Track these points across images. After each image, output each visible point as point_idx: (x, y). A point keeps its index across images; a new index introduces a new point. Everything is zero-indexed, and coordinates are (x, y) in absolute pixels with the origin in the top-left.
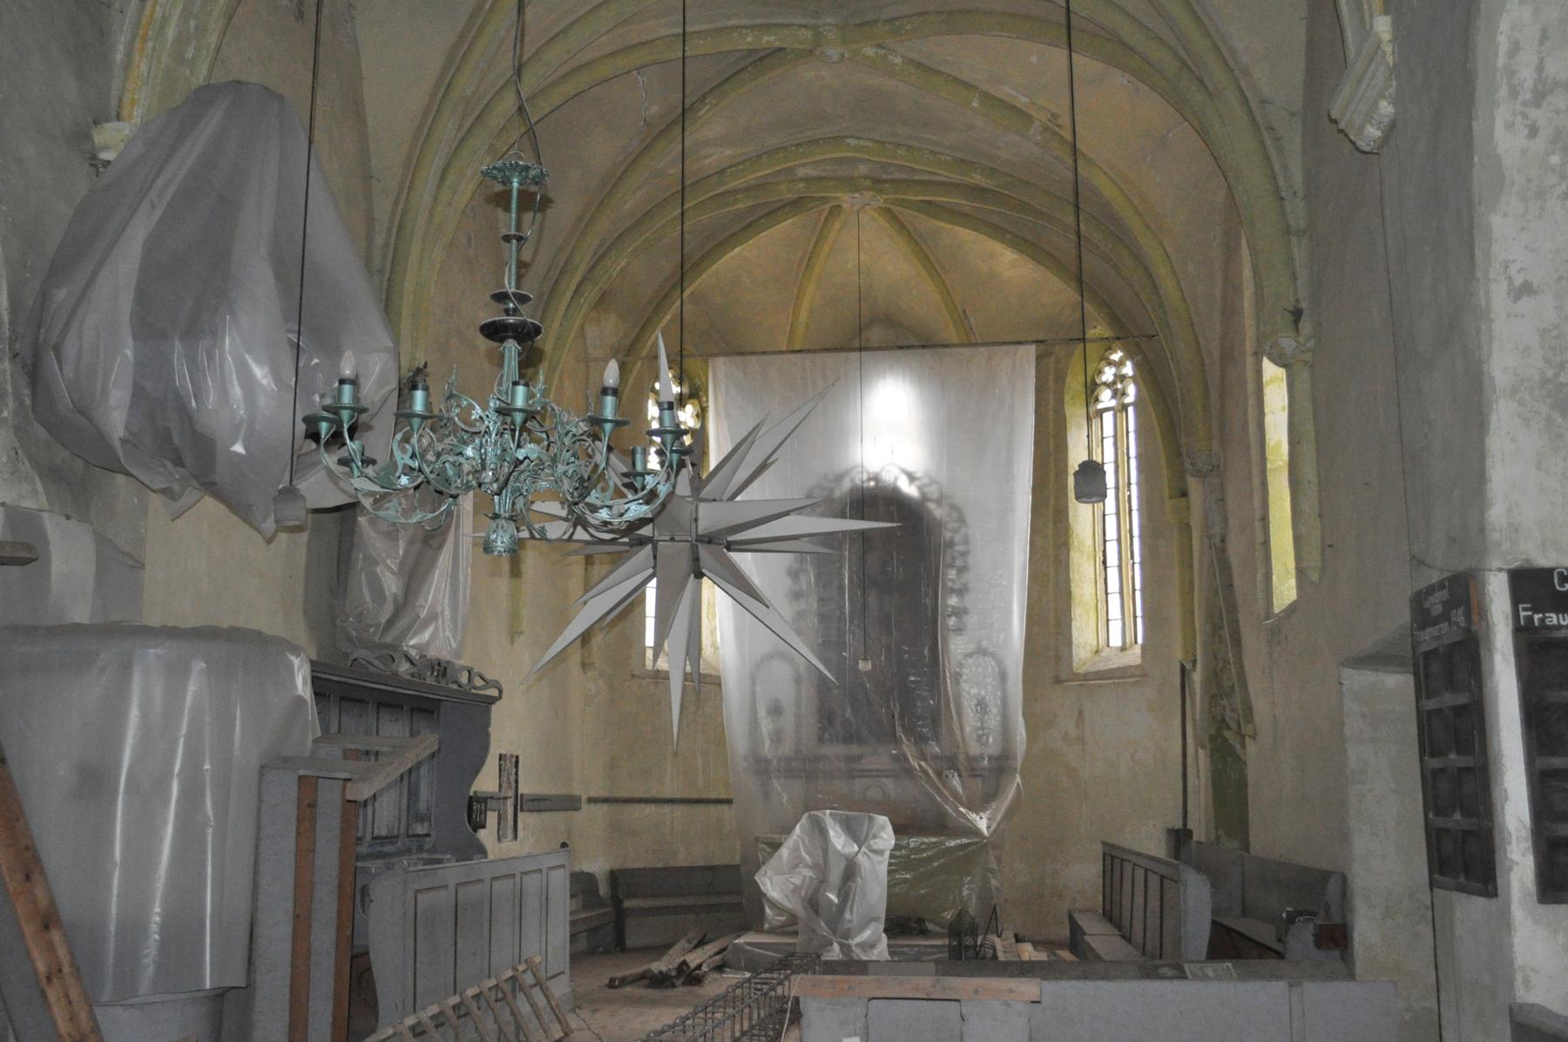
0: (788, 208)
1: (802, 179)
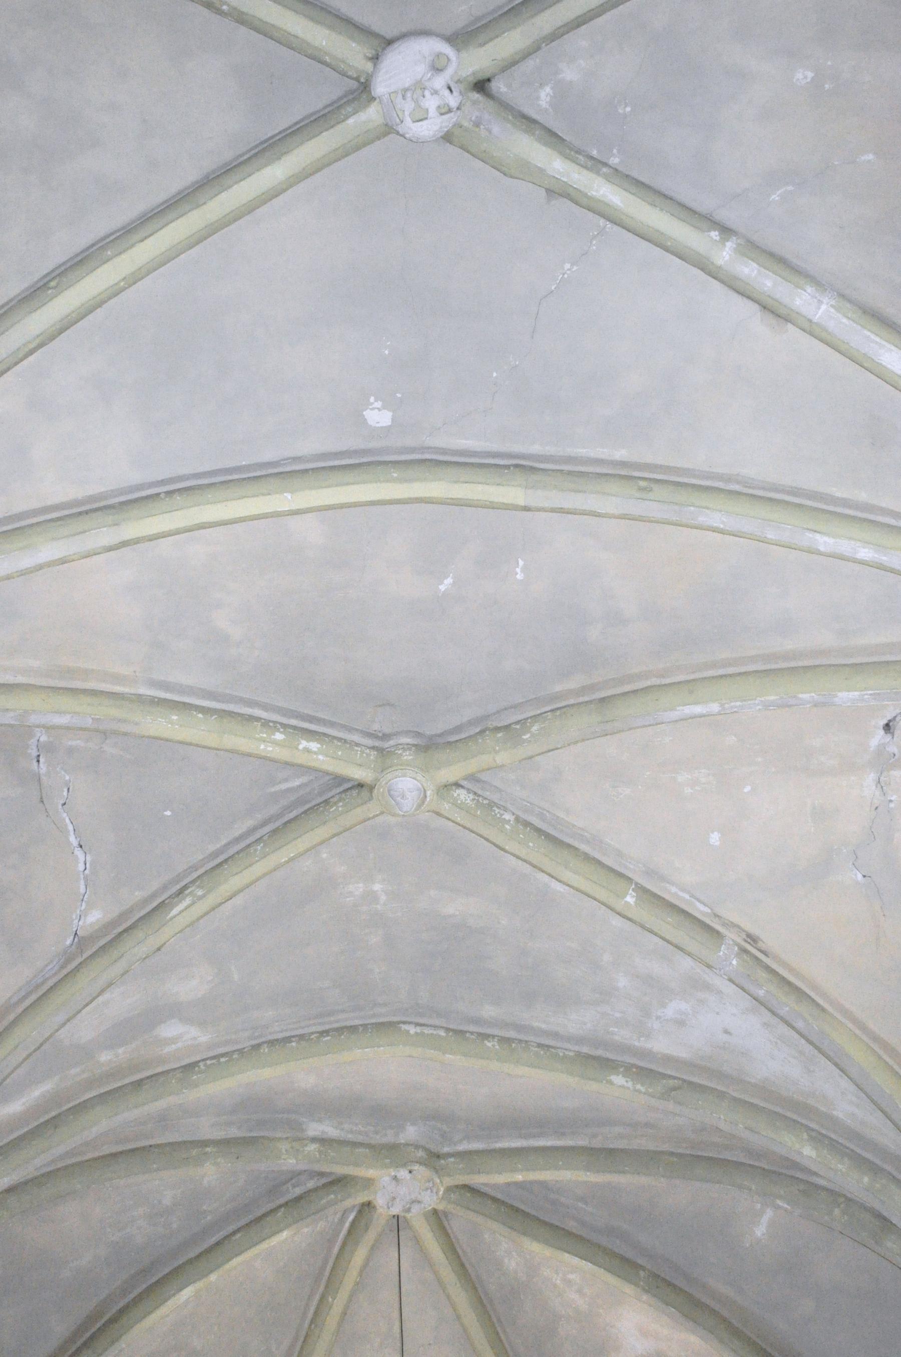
0: (283, 1209)
1: (314, 1140)
